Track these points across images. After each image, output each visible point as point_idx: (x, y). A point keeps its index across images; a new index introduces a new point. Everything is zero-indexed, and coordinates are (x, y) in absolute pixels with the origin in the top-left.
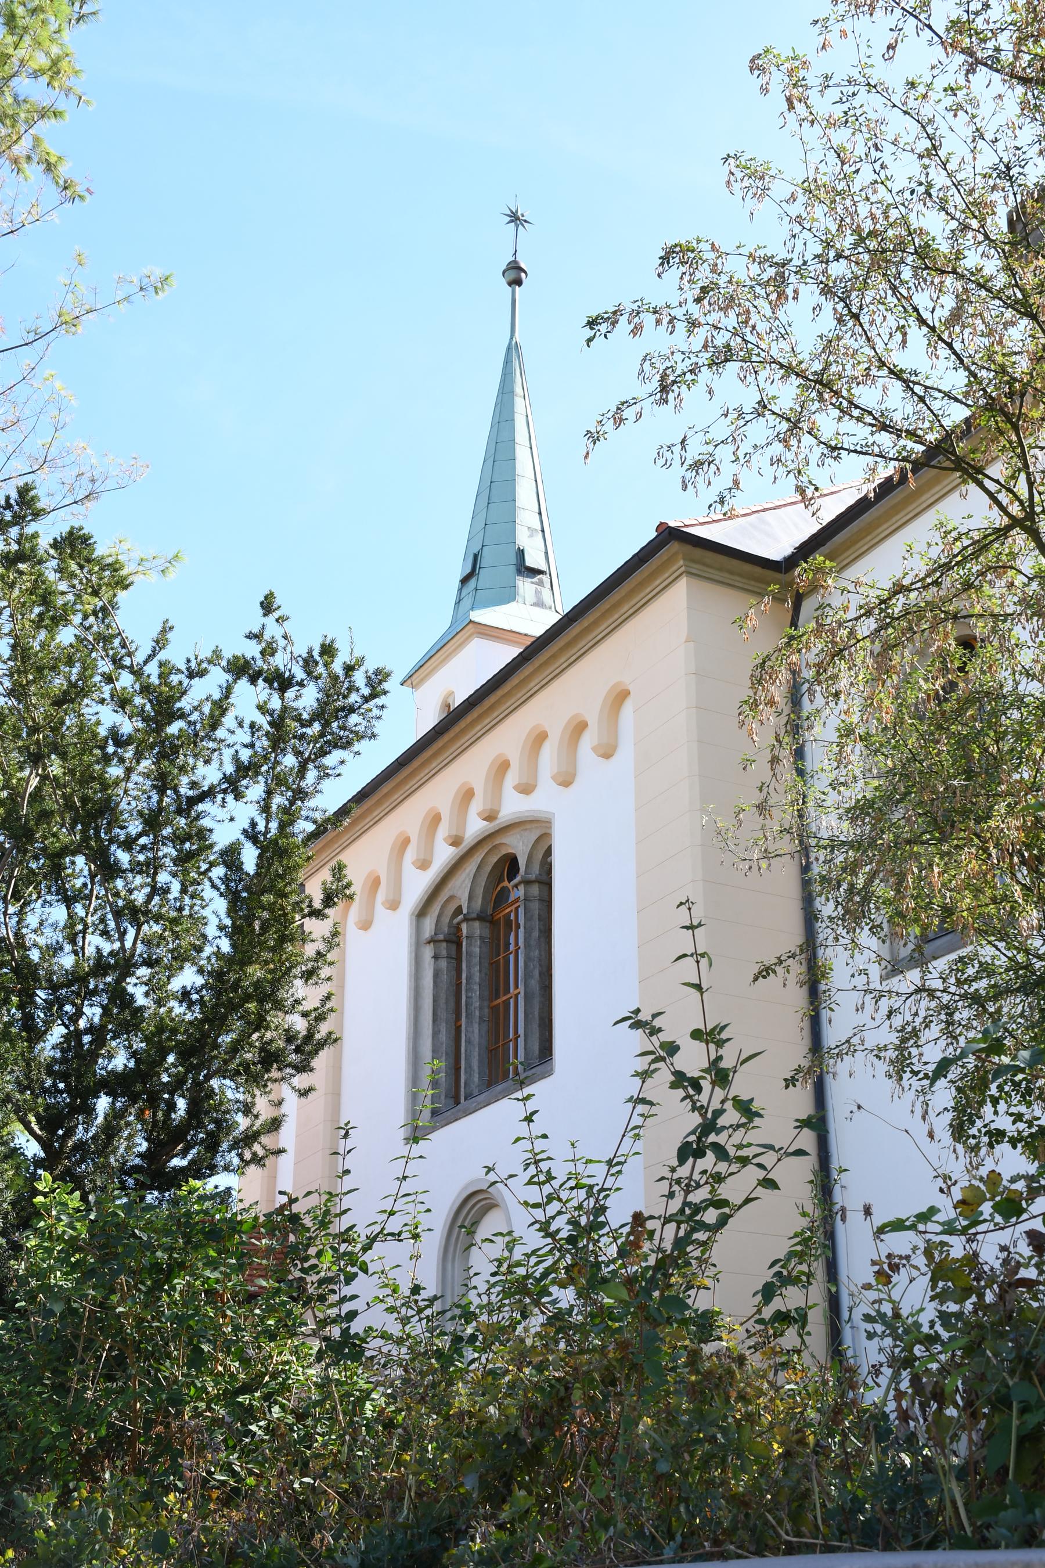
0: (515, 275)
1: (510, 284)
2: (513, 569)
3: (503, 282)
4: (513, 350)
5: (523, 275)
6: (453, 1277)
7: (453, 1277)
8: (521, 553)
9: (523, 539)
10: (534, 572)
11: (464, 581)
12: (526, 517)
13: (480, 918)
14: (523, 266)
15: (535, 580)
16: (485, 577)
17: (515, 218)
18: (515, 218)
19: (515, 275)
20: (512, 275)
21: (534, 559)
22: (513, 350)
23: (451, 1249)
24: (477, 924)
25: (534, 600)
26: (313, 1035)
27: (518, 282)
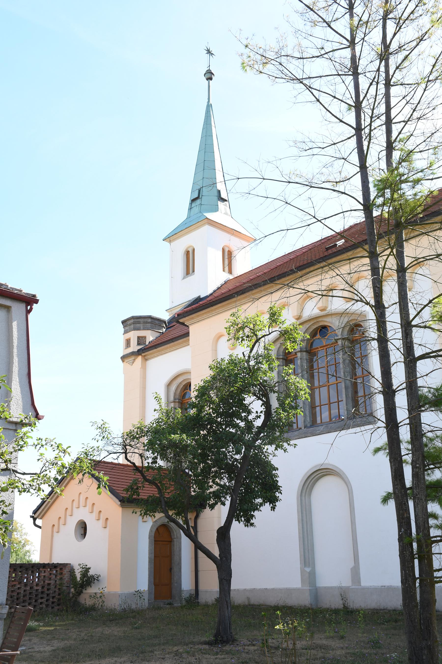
0: (209, 75)
1: (207, 79)
2: (216, 198)
3: (204, 79)
4: (209, 106)
5: (213, 76)
6: (305, 503)
7: (305, 503)
8: (219, 192)
9: (220, 186)
10: (224, 200)
11: (193, 200)
12: (219, 177)
13: (306, 351)
14: (213, 72)
15: (224, 203)
16: (204, 200)
17: (209, 52)
18: (209, 52)
19: (209, 75)
20: (208, 75)
21: (223, 195)
22: (209, 106)
23: (304, 491)
24: (304, 353)
25: (224, 212)
26: (139, 350)
27: (211, 79)
